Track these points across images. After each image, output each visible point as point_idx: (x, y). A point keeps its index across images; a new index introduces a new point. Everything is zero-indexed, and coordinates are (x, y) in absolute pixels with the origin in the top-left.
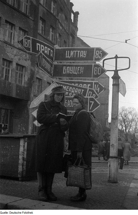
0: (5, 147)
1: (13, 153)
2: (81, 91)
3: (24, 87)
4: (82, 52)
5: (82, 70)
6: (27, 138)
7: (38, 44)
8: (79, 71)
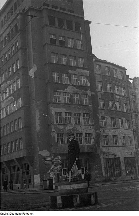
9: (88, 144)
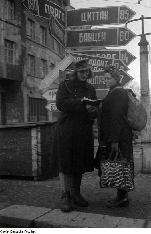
0: (12, 140)
1: (23, 146)
2: (105, 63)
3: (15, 66)
4: (102, 13)
5: (104, 37)
6: (39, 128)
7: (46, 5)
8: (101, 38)
9: (8, 62)
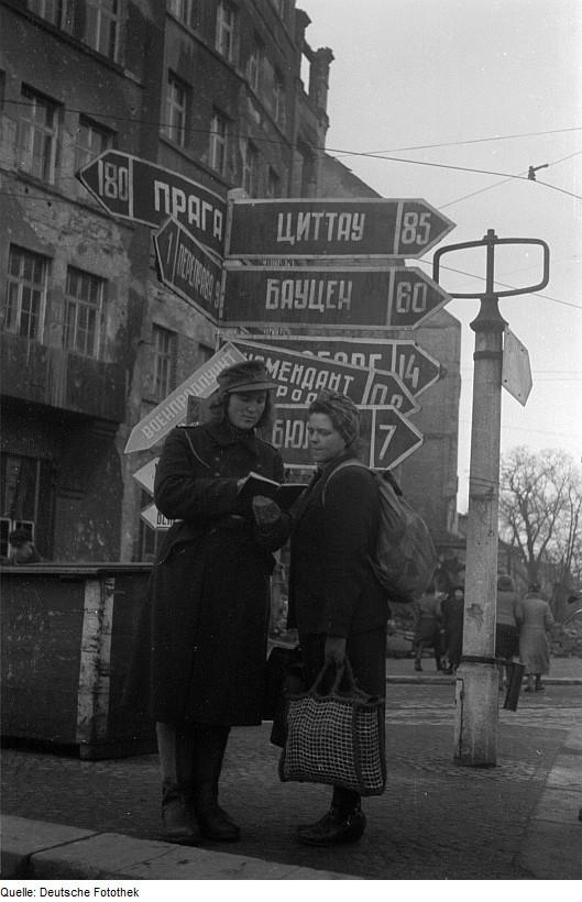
0: (20, 617)
1: (54, 640)
2: (343, 381)
3: (101, 364)
4: (345, 219)
5: (345, 296)
6: (113, 581)
7: (158, 185)
8: (335, 299)
